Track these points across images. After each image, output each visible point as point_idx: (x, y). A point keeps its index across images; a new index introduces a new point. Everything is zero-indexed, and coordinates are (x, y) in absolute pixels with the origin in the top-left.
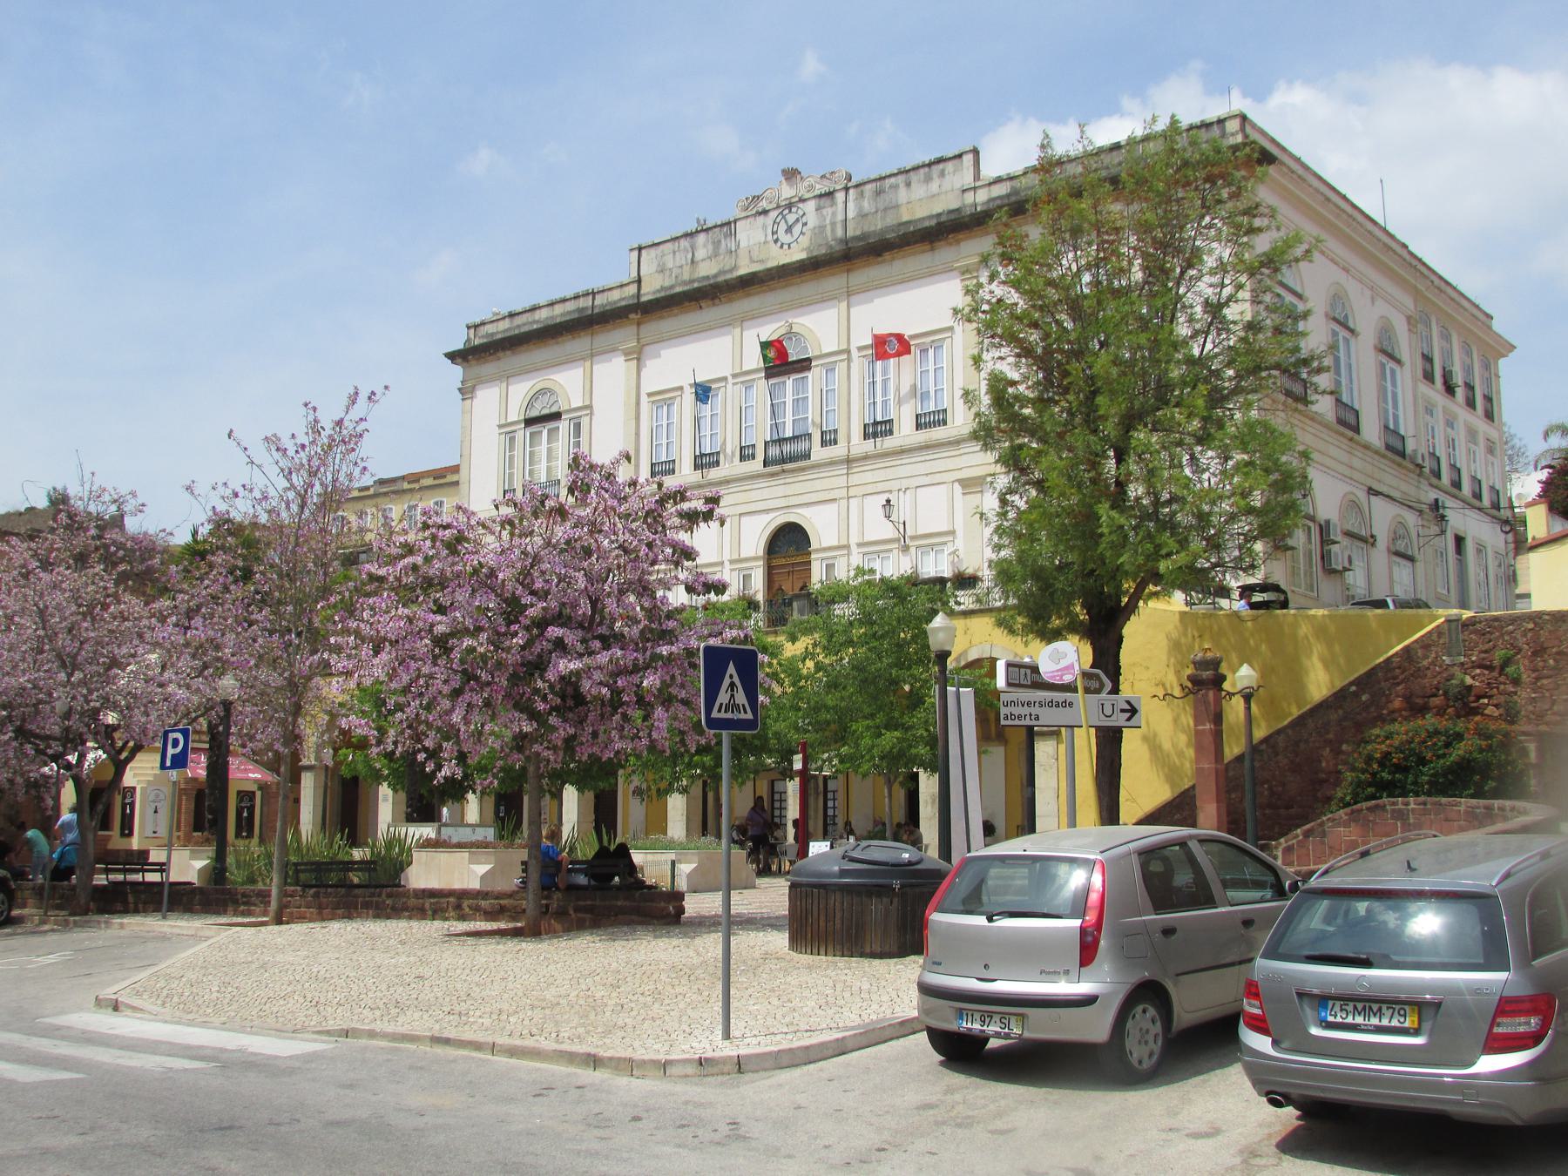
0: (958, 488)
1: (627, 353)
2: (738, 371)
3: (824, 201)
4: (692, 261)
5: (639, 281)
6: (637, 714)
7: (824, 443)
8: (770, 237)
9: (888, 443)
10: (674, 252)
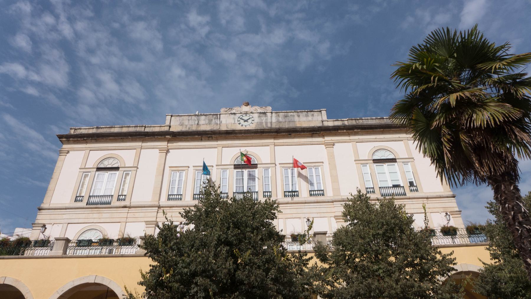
0: (333, 219)
1: (161, 150)
2: (84, 167)
3: (261, 115)
4: (198, 124)
5: (170, 127)
6: (204, 285)
7: (118, 200)
8: (236, 122)
9: (296, 199)
10: (189, 120)
